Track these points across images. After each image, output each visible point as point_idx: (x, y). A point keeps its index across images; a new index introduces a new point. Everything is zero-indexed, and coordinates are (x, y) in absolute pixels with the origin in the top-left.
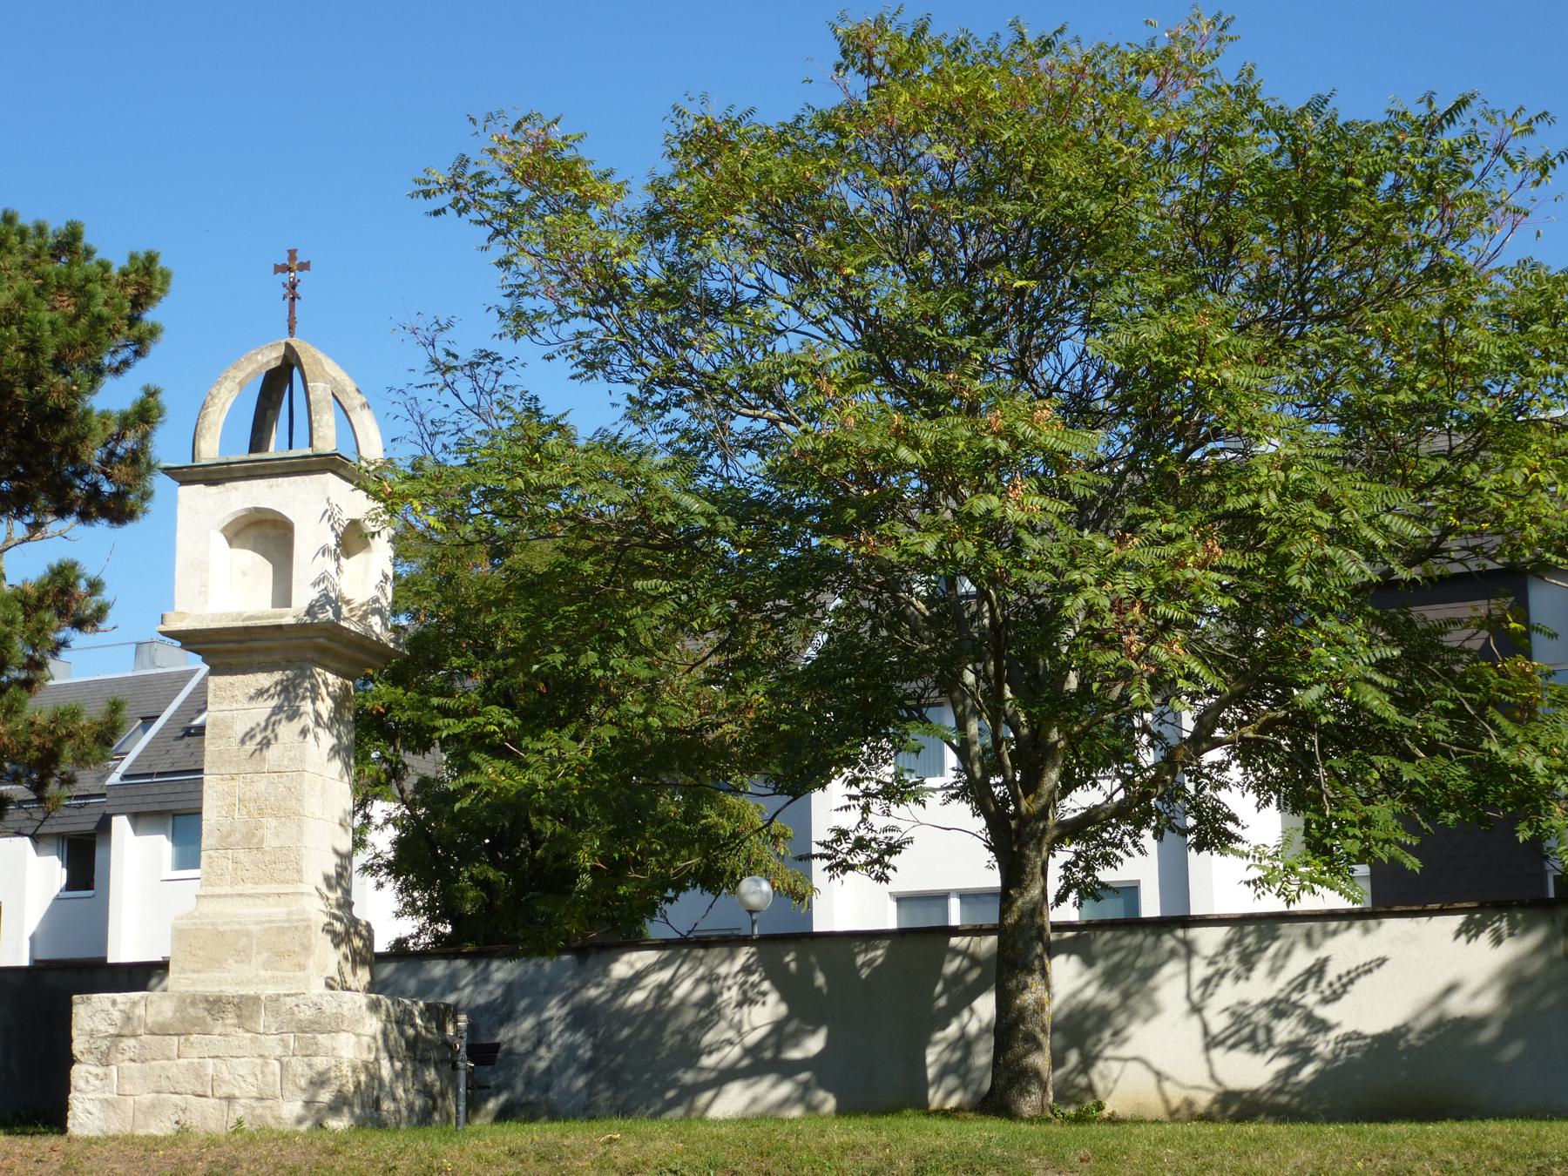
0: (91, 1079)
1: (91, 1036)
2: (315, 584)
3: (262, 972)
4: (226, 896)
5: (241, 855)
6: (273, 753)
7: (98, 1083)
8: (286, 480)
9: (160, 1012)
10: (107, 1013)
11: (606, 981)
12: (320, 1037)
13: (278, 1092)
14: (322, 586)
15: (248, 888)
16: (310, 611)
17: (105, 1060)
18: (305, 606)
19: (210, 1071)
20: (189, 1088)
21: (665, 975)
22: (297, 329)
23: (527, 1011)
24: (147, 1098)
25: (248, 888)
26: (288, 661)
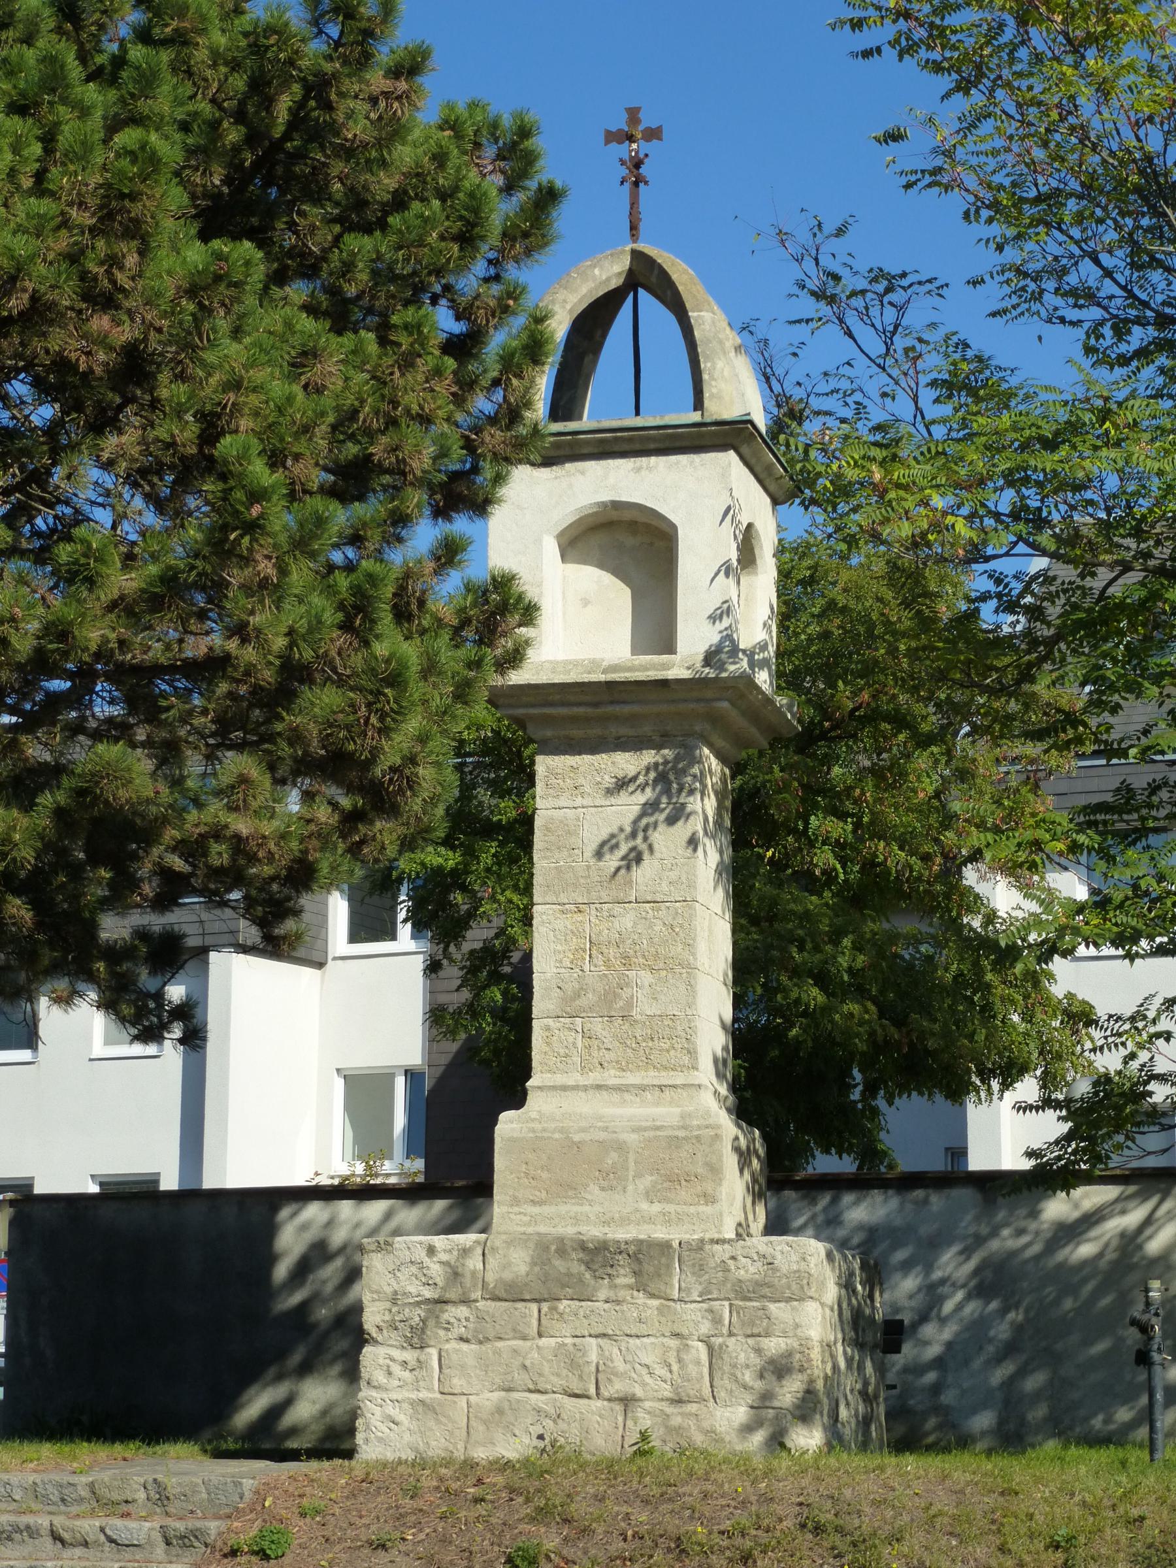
0: (396, 1369)
1: (394, 1302)
2: (714, 618)
3: (644, 1206)
4: (575, 1088)
5: (598, 1026)
6: (643, 874)
7: (406, 1375)
8: (683, 459)
9: (506, 1266)
10: (421, 1266)
11: (1033, 1226)
12: (773, 1307)
13: (707, 1391)
14: (726, 622)
15: (611, 1077)
16: (710, 658)
17: (417, 1339)
18: (701, 649)
19: (593, 1357)
20: (559, 1383)
21: (1133, 1218)
22: (642, 226)
23: (906, 1267)
24: (489, 1398)
25: (611, 1077)
26: (664, 735)
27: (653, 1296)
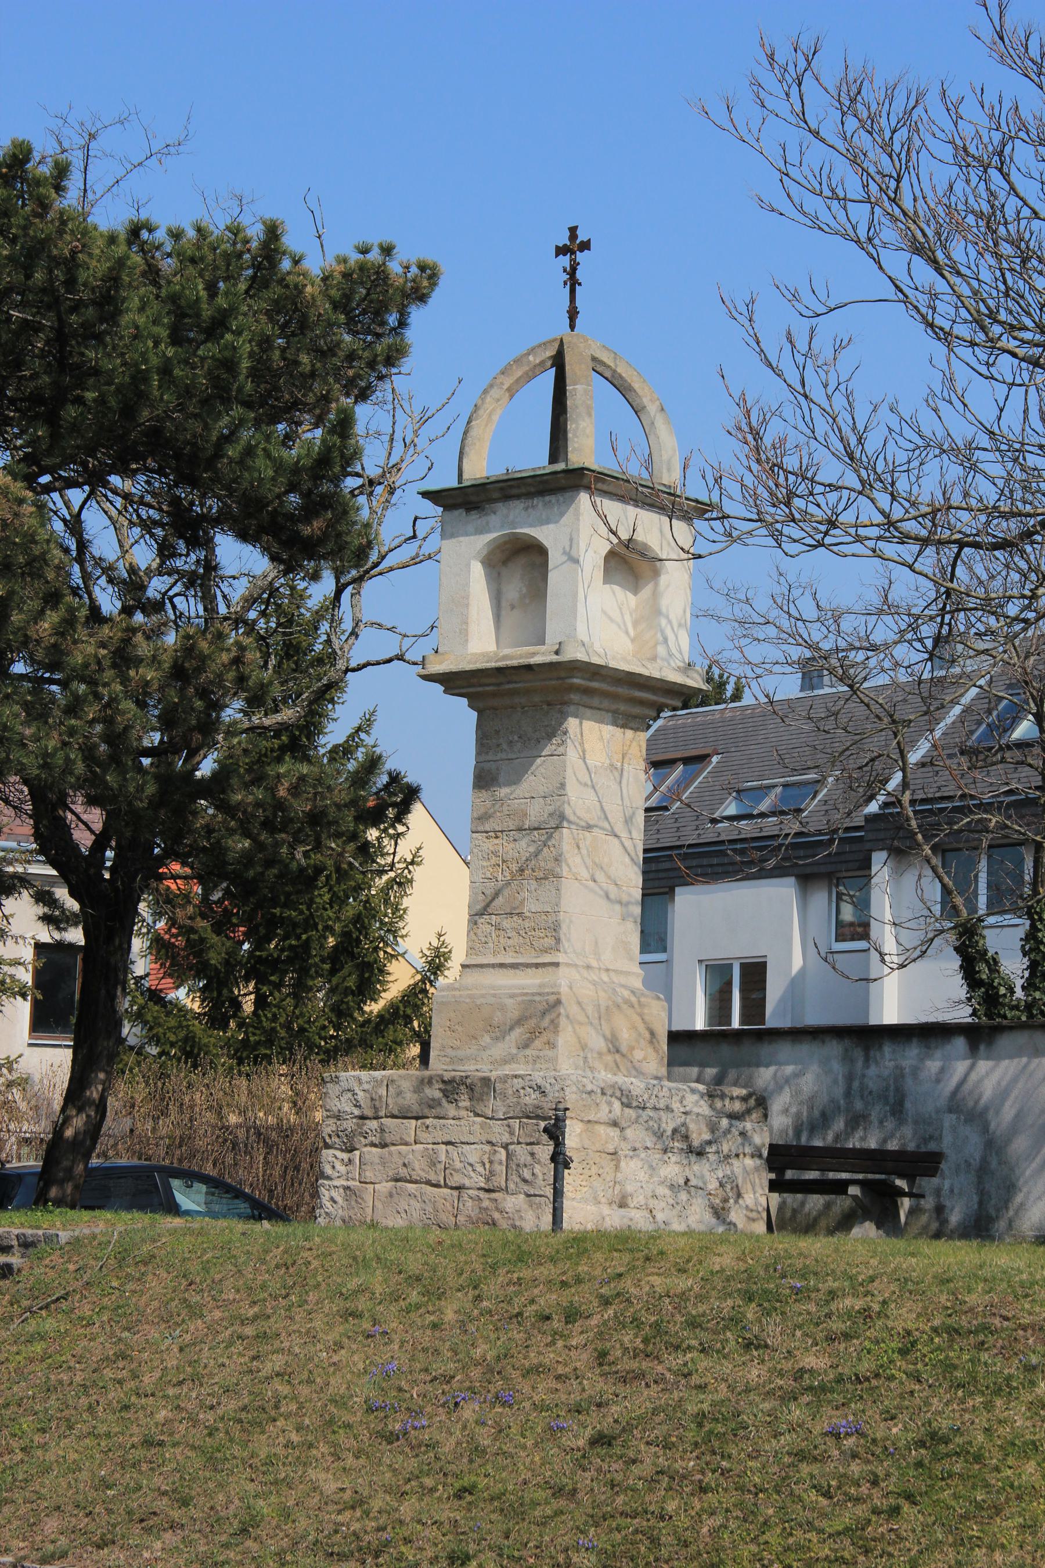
0: (339, 1166)
19: (443, 1157)
27: (477, 1115)
